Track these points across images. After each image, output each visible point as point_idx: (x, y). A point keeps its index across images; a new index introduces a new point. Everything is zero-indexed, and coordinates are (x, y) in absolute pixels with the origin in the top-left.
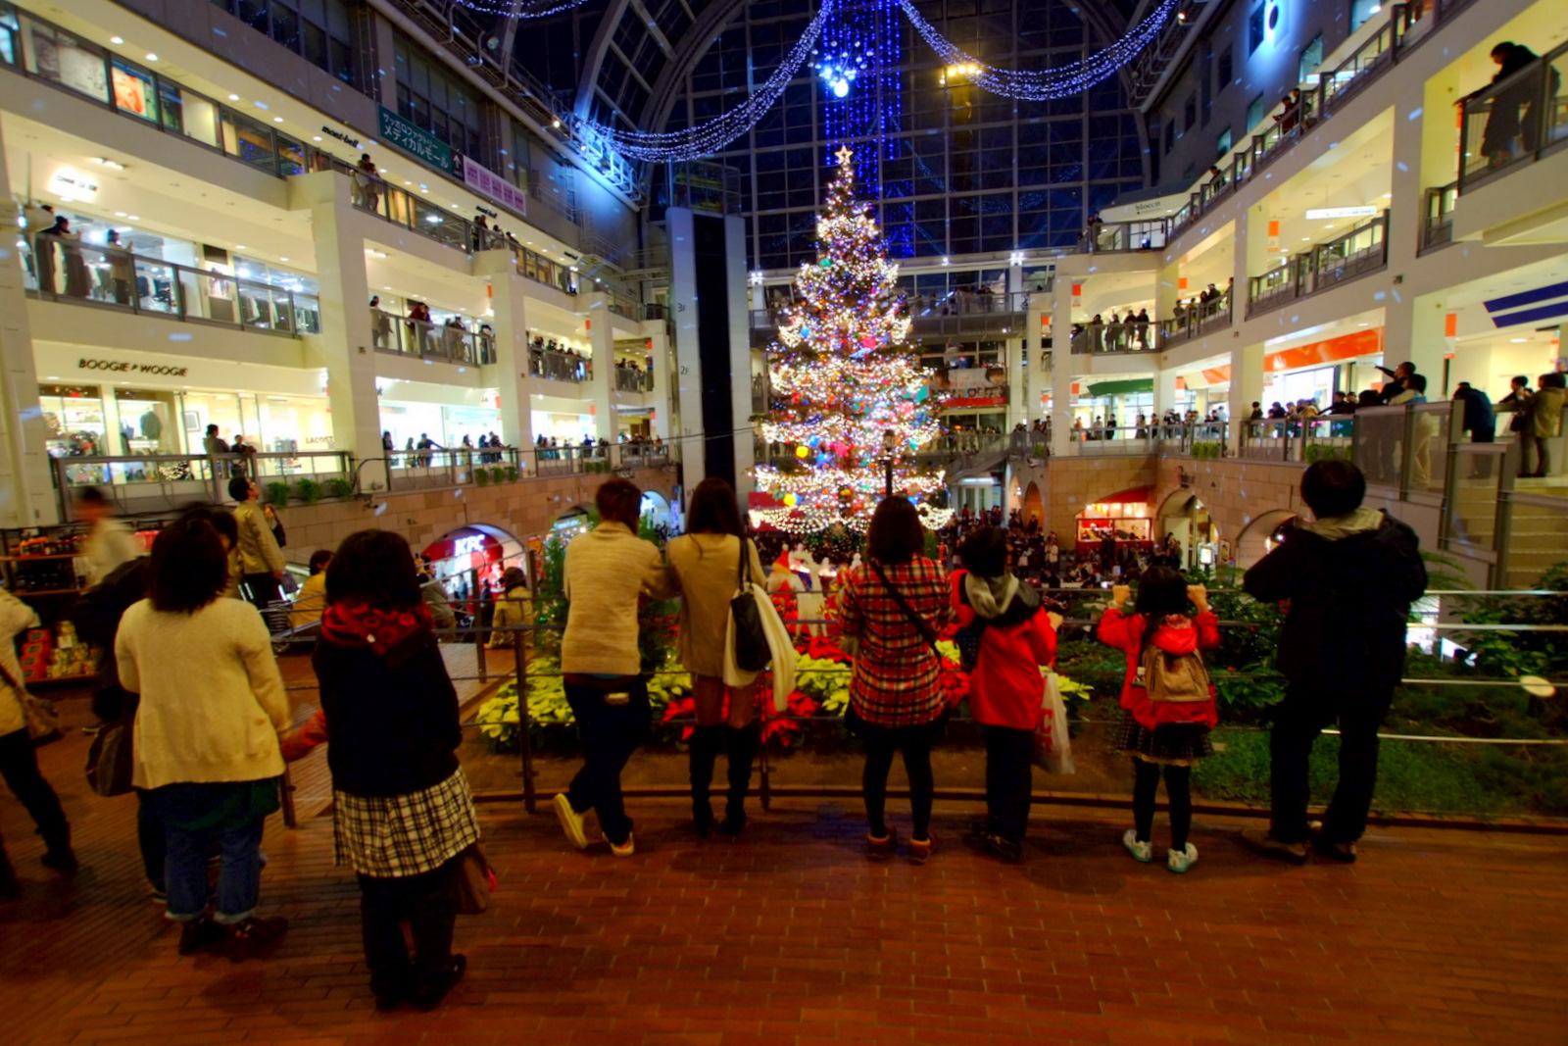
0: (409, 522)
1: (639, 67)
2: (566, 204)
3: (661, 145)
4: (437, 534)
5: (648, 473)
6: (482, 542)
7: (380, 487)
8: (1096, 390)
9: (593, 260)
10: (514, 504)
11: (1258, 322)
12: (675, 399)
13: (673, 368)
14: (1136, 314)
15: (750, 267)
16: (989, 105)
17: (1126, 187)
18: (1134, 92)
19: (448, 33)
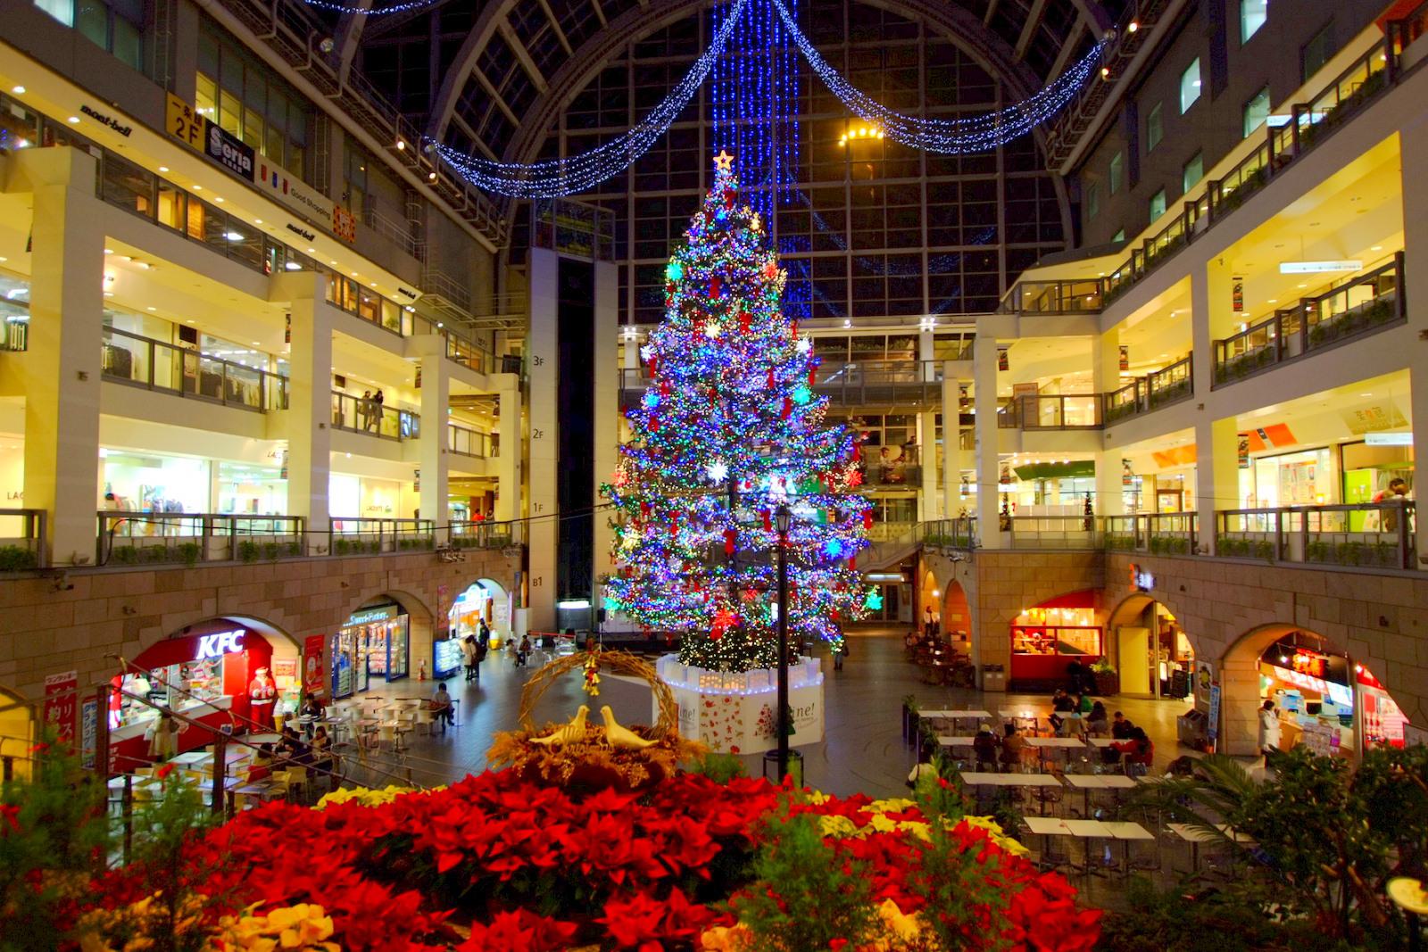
1: (507, 97)
4: (171, 625)
6: (239, 641)
8: (1027, 473)
9: (436, 302)
10: (291, 590)
12: (524, 468)
15: (623, 320)
16: (896, 159)
17: (1044, 251)
18: (1053, 153)
19: (271, 27)
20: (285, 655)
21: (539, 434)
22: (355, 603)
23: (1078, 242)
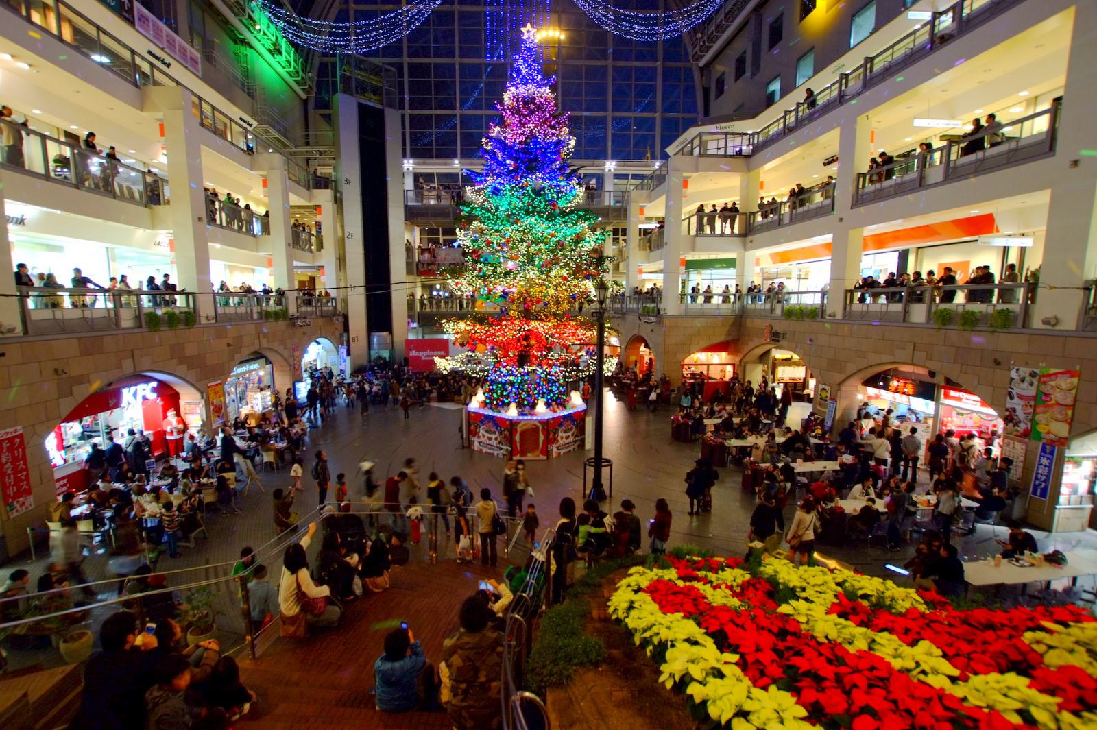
0: (56, 371)
2: (239, 75)
3: (331, 34)
5: (320, 322)
6: (154, 390)
7: (12, 330)
9: (266, 131)
10: (191, 350)
11: (862, 210)
12: (341, 260)
13: (340, 234)
14: (729, 206)
15: (404, 156)
20: (190, 400)
21: (351, 235)
22: (239, 357)
23: (706, 113)
